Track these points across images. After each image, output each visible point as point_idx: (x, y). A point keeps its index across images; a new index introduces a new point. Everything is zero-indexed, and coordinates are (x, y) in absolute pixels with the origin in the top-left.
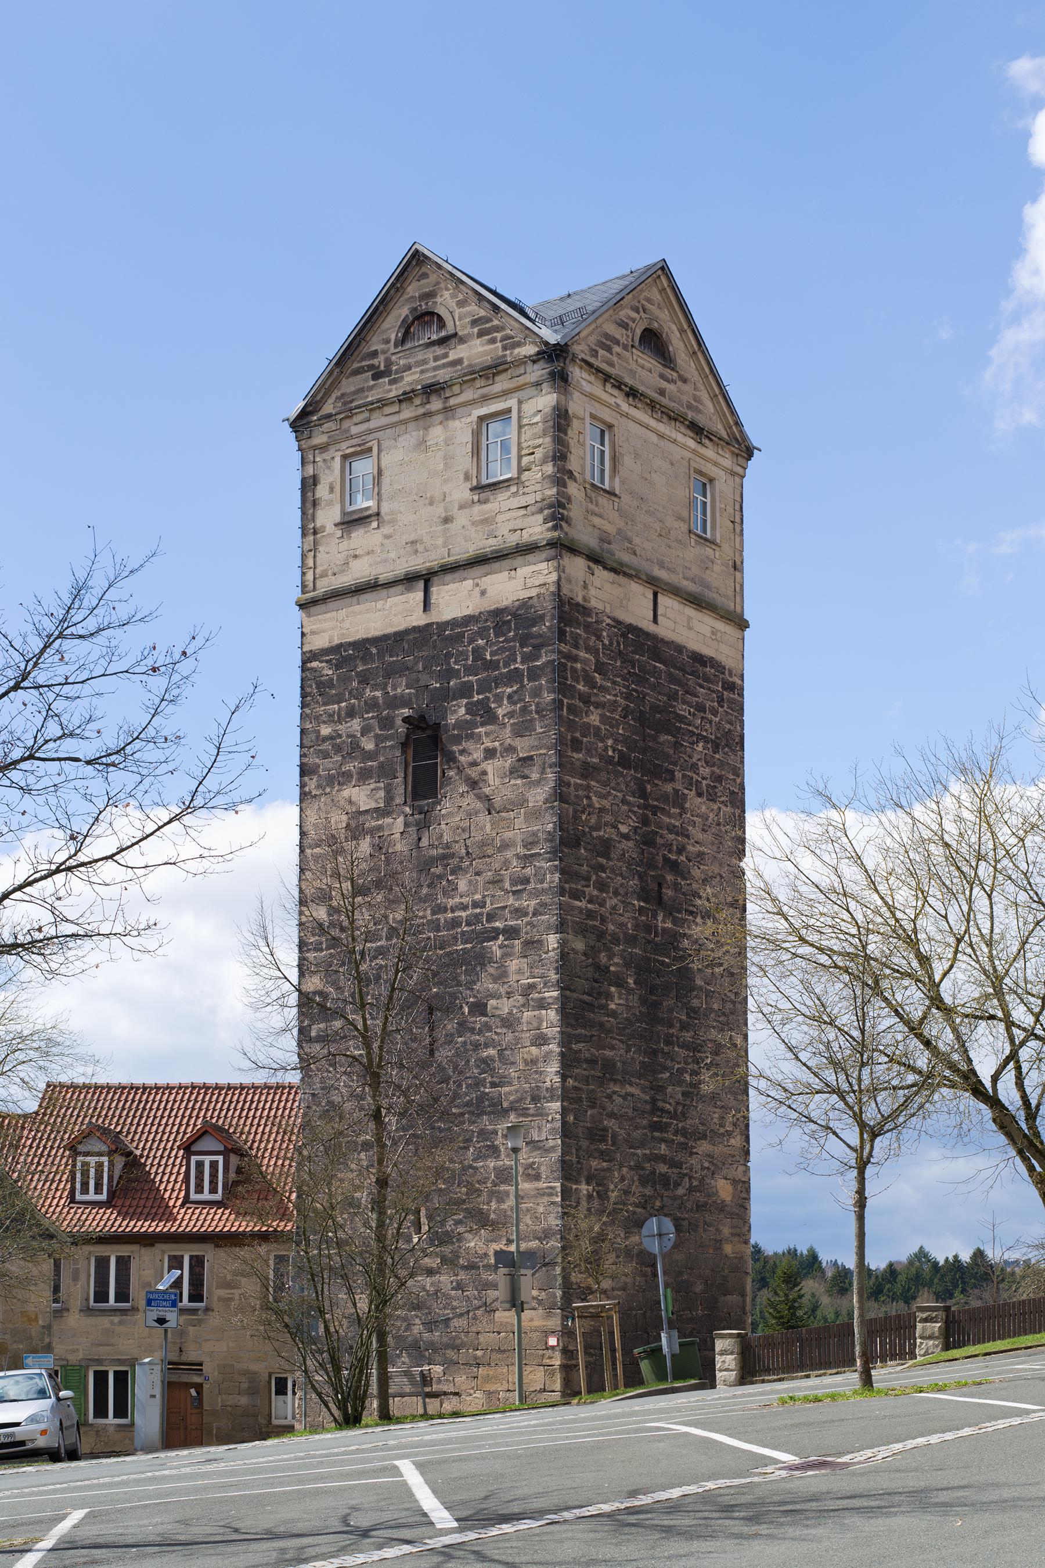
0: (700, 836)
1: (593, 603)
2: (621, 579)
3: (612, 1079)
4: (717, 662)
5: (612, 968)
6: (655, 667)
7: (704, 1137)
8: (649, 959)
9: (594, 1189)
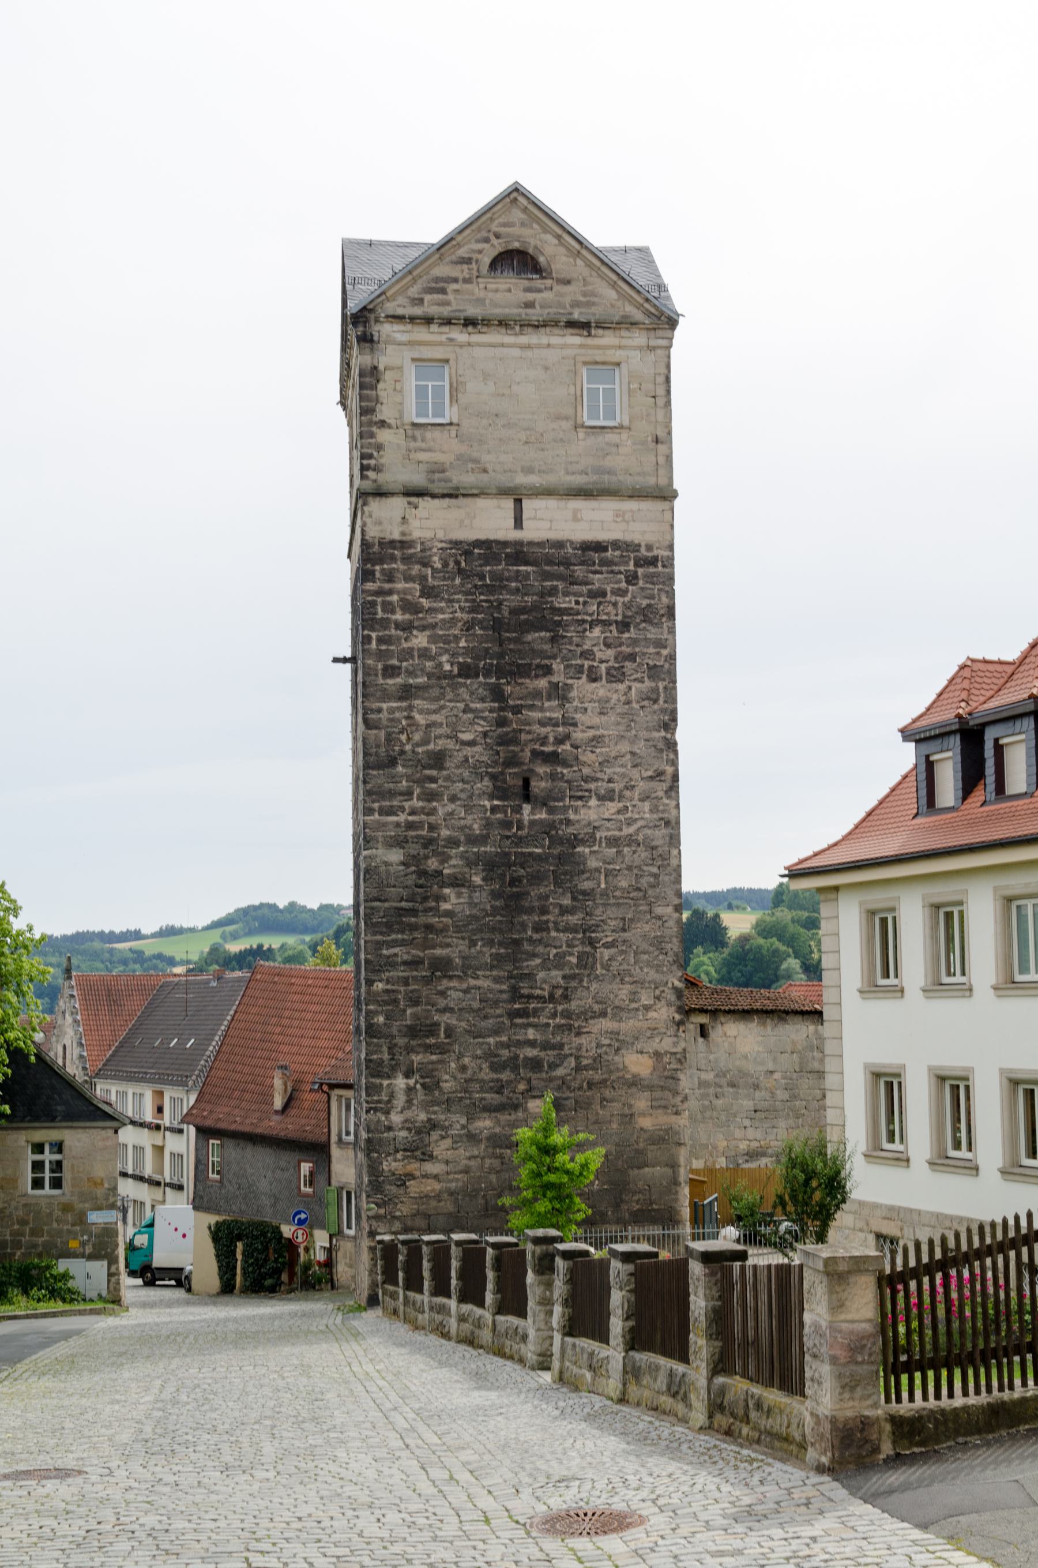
1: (416, 534)
2: (461, 501)
3: (445, 976)
4: (625, 543)
5: (446, 871)
7: (603, 1014)
8: (508, 854)
9: (417, 1082)
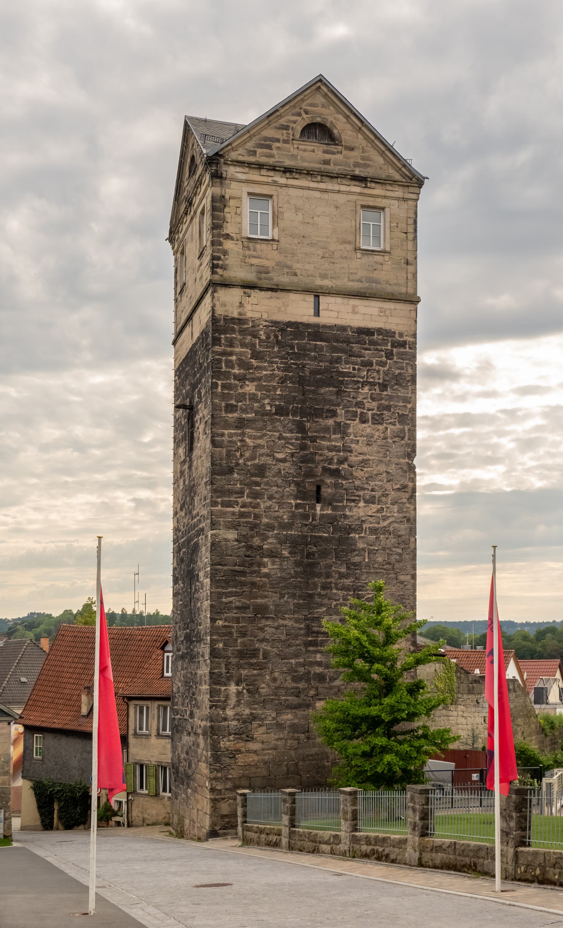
0: (365, 449)
1: (249, 315)
2: (280, 294)
3: (263, 618)
4: (386, 330)
5: (265, 547)
6: (316, 345)
